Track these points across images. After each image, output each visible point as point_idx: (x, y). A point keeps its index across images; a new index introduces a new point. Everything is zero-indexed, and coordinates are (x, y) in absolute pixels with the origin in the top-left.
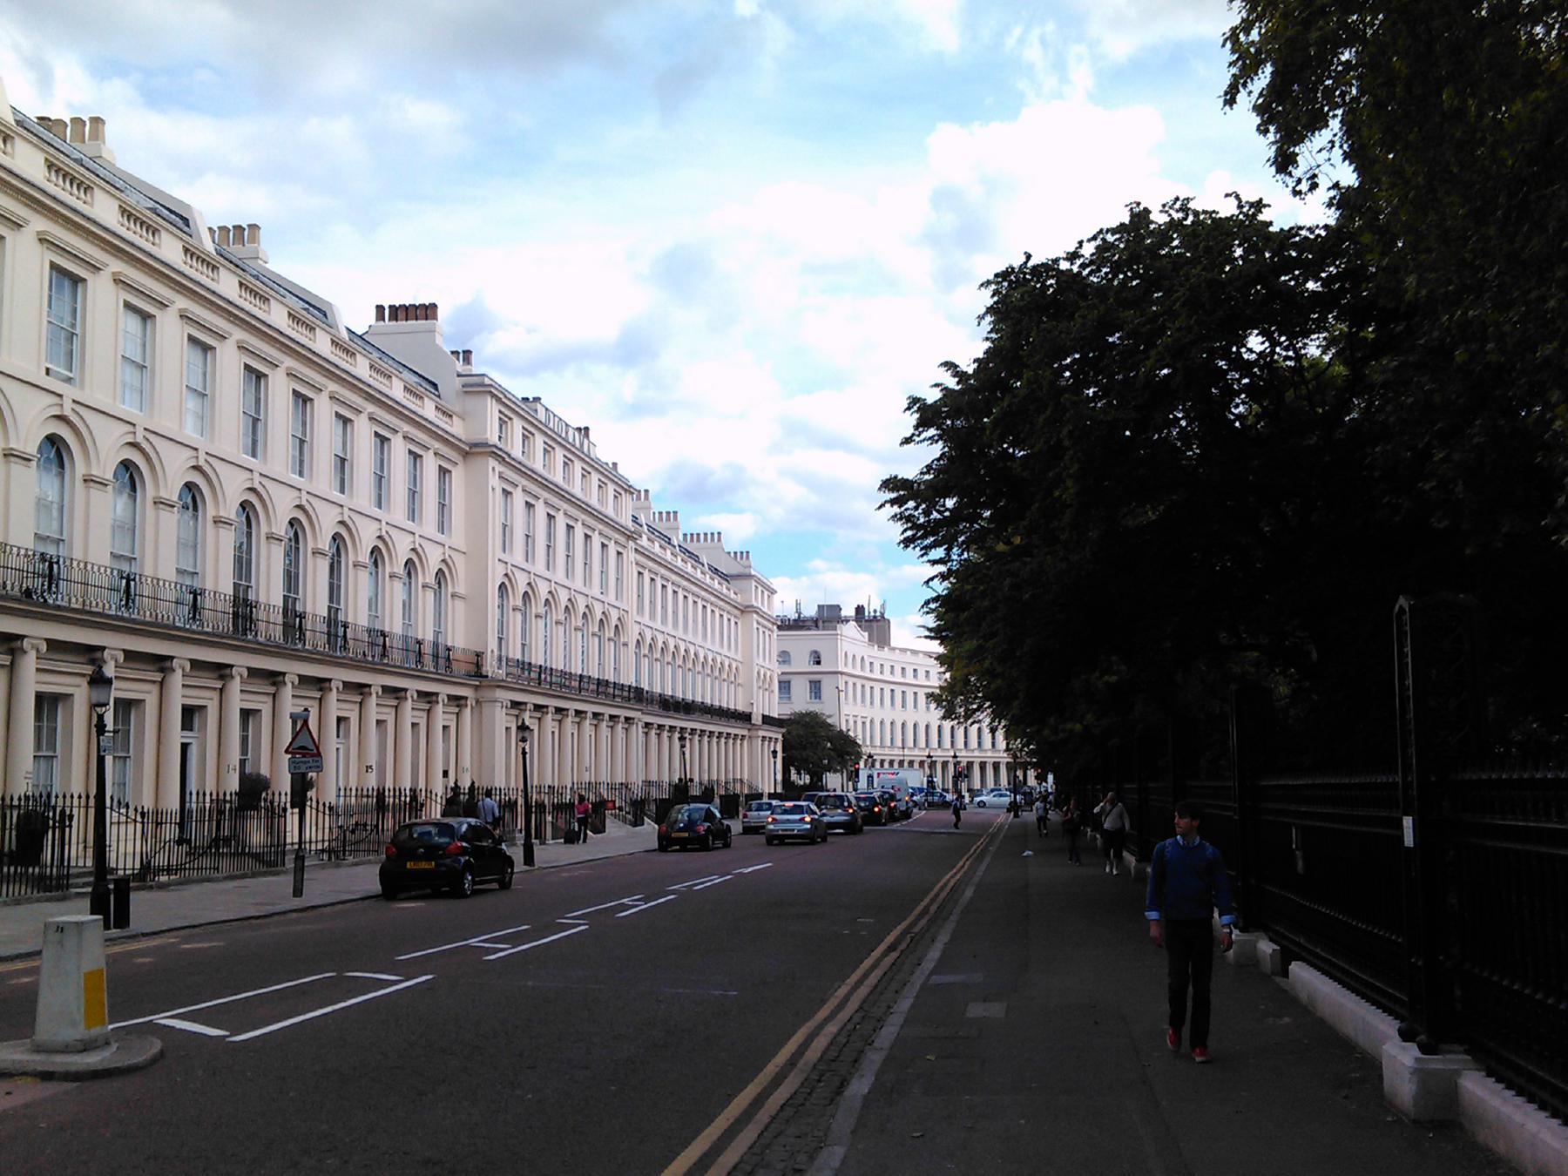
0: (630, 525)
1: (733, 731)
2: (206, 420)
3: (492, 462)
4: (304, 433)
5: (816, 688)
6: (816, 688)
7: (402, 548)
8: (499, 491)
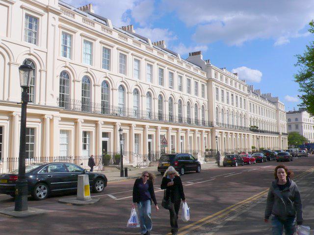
1: (266, 136)
2: (151, 80)
3: (213, 82)
5: (297, 127)
6: (297, 127)
7: (145, 89)
8: (215, 88)
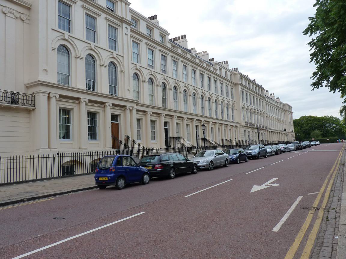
2: (177, 74)
4: (165, 64)
7: (207, 95)
8: (241, 91)
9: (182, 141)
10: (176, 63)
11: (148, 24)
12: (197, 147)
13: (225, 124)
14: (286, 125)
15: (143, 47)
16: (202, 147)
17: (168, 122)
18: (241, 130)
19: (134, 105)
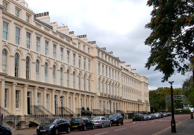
0: (121, 68)
8: (98, 63)
9: (42, 109)
10: (7, 24)
11: (16, 6)
12: (56, 115)
13: (82, 95)
14: (142, 95)
15: (12, 27)
16: (60, 115)
17: (8, 89)
18: (96, 100)
19: (3, 78)
